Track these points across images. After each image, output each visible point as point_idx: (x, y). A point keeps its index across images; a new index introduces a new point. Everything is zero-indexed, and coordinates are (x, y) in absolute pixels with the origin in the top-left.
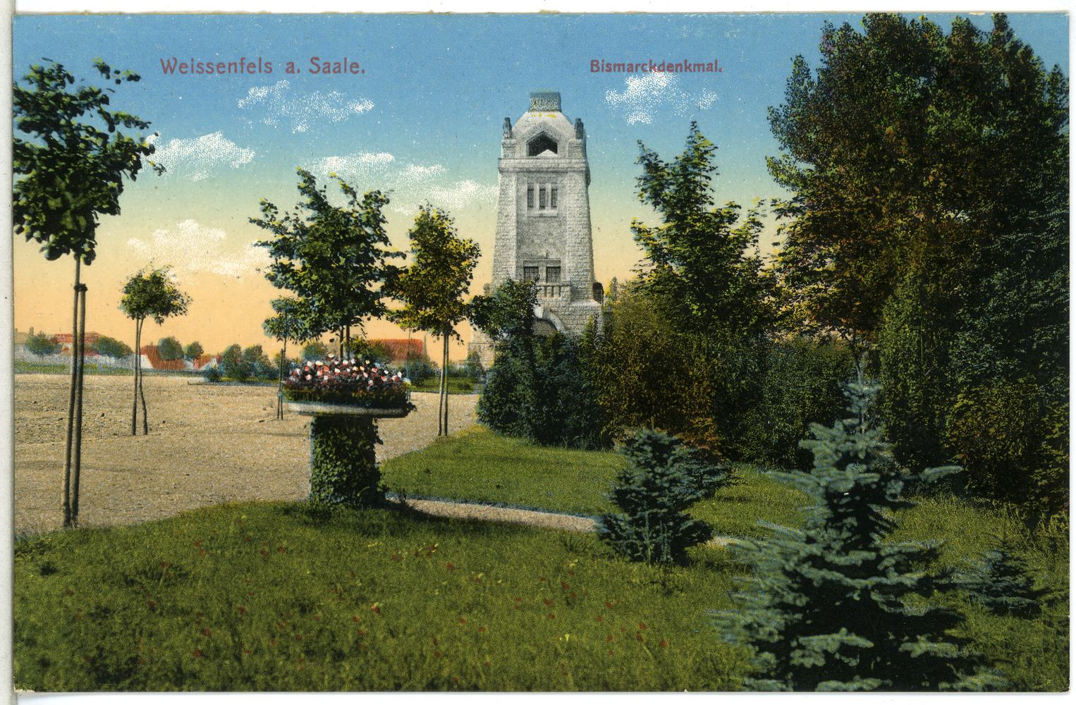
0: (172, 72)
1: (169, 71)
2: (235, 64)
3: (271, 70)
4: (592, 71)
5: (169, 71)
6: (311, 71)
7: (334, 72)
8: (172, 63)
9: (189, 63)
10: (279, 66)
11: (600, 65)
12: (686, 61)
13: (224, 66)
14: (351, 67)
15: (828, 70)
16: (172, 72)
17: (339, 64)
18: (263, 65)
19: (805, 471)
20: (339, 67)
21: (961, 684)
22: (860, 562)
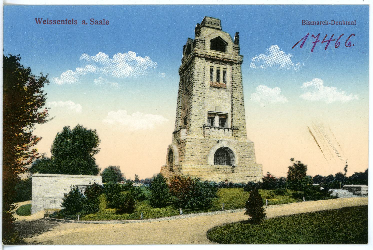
0: (40, 23)
1: (39, 23)
2: (341, 22)
3: (77, 23)
4: (303, 24)
5: (39, 23)
6: (91, 24)
7: (352, 24)
8: (40, 20)
9: (47, 20)
10: (80, 22)
11: (306, 23)
12: (326, 21)
13: (46, 21)
14: (106, 22)
15: (165, 186)
16: (40, 23)
17: (319, 22)
18: (74, 21)
19: (162, 177)
20: (102, 22)
21: (33, 239)
22: (262, 181)
